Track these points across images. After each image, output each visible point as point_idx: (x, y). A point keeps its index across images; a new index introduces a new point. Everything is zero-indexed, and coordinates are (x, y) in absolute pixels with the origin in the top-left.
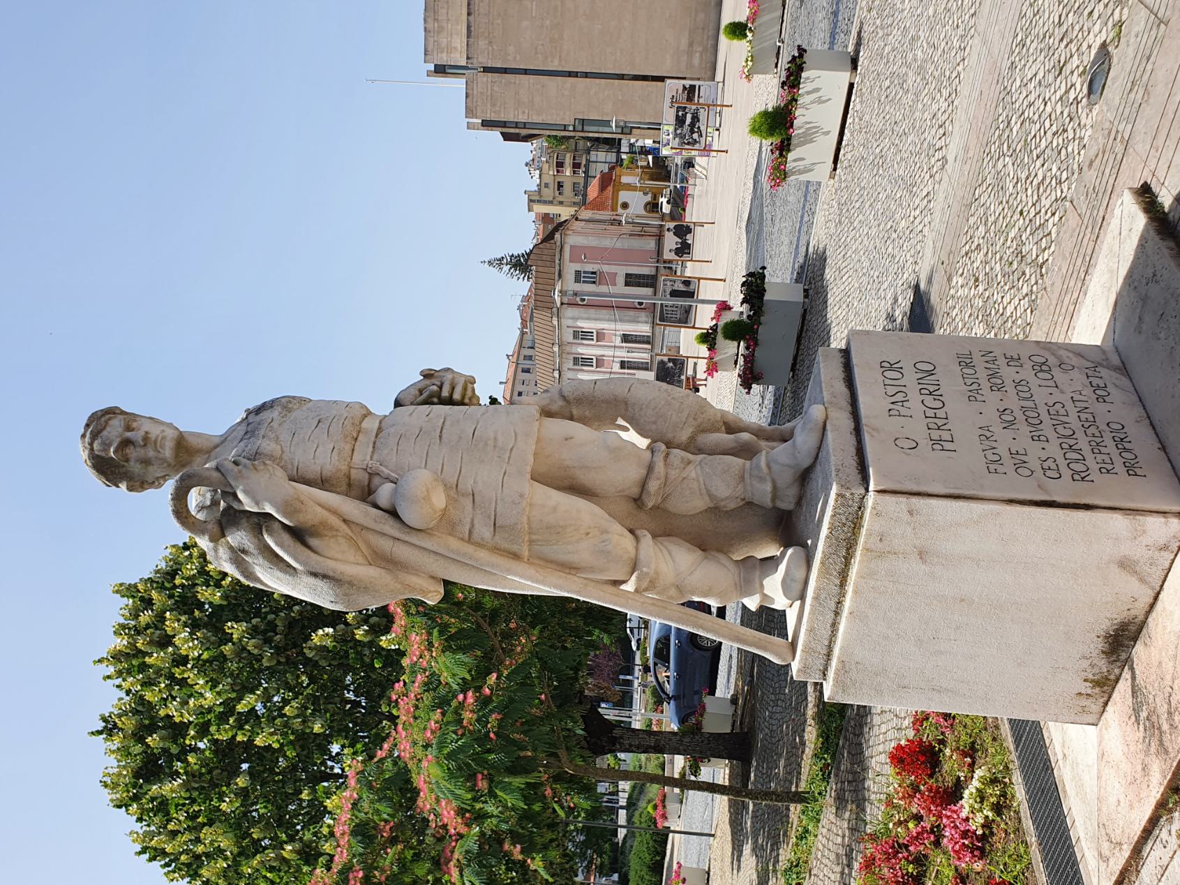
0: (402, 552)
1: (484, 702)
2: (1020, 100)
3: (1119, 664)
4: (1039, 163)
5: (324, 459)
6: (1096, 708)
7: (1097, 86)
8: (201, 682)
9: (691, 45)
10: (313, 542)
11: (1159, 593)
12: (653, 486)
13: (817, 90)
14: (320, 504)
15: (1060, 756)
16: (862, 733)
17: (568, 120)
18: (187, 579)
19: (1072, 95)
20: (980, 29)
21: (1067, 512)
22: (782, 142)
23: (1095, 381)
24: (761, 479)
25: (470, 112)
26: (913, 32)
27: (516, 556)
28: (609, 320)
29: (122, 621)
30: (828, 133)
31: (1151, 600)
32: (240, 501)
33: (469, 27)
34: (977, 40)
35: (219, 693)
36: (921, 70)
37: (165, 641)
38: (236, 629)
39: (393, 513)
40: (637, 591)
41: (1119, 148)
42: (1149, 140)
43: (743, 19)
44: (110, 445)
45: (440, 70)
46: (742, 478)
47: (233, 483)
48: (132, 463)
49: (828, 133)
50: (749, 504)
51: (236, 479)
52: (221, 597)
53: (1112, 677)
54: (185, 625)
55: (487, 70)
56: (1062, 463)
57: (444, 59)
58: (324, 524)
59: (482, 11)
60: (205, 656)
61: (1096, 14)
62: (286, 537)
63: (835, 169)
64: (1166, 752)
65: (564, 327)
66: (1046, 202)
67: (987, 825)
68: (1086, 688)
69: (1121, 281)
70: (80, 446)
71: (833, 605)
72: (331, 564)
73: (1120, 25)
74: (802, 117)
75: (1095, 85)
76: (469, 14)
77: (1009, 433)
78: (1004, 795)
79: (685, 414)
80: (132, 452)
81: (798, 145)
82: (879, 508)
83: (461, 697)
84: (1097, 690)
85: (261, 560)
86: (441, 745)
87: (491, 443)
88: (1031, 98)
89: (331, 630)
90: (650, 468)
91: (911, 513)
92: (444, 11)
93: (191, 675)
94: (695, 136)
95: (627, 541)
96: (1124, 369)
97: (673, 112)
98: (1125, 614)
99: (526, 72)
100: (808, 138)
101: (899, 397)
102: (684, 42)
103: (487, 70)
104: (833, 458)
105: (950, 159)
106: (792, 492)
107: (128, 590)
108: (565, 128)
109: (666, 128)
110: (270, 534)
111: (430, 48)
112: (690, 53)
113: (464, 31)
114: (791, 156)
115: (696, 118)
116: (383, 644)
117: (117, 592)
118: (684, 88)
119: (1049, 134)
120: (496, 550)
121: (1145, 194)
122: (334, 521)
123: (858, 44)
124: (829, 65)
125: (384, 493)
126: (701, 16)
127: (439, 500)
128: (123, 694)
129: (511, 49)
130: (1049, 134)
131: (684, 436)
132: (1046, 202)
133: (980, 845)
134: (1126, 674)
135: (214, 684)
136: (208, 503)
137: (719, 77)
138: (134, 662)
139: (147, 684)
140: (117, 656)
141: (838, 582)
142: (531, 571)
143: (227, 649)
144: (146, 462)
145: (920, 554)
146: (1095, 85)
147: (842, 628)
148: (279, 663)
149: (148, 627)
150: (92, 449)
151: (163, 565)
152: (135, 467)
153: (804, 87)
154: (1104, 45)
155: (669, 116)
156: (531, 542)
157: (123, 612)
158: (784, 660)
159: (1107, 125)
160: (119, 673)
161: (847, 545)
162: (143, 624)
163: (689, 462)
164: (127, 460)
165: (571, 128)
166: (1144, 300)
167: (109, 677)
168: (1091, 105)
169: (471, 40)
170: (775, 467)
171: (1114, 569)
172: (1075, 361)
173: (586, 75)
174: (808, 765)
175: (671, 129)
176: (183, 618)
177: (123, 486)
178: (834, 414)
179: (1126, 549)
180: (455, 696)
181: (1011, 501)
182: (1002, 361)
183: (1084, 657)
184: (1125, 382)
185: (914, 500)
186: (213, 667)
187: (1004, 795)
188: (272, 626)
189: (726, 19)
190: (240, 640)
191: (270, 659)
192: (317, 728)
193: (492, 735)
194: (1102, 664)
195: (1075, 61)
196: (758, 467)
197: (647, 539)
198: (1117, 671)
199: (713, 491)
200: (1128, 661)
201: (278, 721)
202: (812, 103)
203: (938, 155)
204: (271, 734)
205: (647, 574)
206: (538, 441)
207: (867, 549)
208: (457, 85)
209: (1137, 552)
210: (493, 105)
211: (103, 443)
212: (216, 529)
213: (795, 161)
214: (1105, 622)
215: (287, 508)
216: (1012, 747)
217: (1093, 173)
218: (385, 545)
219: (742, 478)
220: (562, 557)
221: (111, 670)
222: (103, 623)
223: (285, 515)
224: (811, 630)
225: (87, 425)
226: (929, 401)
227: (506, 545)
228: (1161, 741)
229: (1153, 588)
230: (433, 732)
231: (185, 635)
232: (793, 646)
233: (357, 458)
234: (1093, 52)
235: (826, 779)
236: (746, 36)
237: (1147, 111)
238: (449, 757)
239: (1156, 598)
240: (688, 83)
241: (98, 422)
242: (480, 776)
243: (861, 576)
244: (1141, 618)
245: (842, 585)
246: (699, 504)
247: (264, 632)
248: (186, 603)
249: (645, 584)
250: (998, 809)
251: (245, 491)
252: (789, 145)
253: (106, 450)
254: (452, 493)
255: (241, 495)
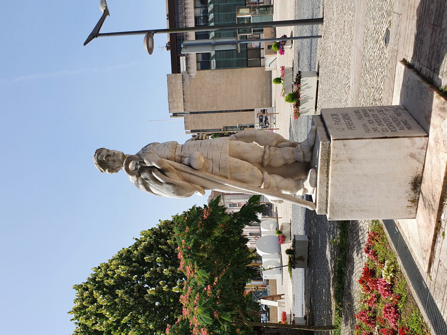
0: (193, 178)
1: (213, 288)
2: (367, 56)
3: (418, 193)
4: (375, 71)
5: (168, 153)
6: (414, 211)
7: (387, 41)
8: (108, 313)
9: (262, 97)
10: (167, 173)
11: (424, 165)
12: (266, 157)
13: (307, 84)
14: (167, 163)
15: (407, 236)
16: (350, 288)
17: (221, 127)
18: (101, 278)
19: (381, 47)
20: (354, 43)
21: (391, 139)
22: (297, 103)
23: (397, 112)
24: (299, 151)
25: (186, 128)
26: (334, 55)
27: (226, 178)
28: (242, 199)
29: (77, 298)
30: (312, 98)
31: (422, 168)
32: (145, 163)
33: (184, 99)
34: (353, 47)
35: (114, 317)
36: (339, 65)
37: (95, 301)
38: (119, 292)
39: (190, 166)
40: (264, 188)
41: (395, 53)
42: (402, 47)
43: (279, 77)
44: (103, 157)
45: (175, 115)
46: (293, 152)
47: (143, 158)
48: (110, 162)
49: (312, 98)
50: (296, 162)
51: (143, 156)
52: (114, 282)
53: (417, 198)
54: (101, 294)
55: (191, 113)
56: (387, 128)
57: (176, 111)
58: (170, 168)
59: (188, 93)
60: (109, 304)
61: (384, 22)
62: (159, 173)
63: (316, 110)
64: (434, 210)
65: (226, 202)
66: (379, 80)
67: (392, 279)
68: (409, 204)
69: (401, 87)
70: (94, 159)
71: (325, 184)
72: (173, 180)
73: (390, 22)
74: (303, 94)
75: (386, 40)
76: (184, 95)
77: (372, 125)
78: (395, 267)
79: (274, 137)
80: (110, 158)
81: (302, 104)
82: (335, 145)
83: (205, 289)
84: (413, 204)
85: (152, 181)
86: (200, 303)
87: (216, 146)
88: (371, 54)
89: (154, 288)
90: (265, 152)
91: (344, 145)
92: (175, 95)
93: (104, 312)
94: (267, 125)
95: (259, 172)
96: (405, 109)
97: (258, 119)
98: (416, 174)
99: (205, 112)
100: (306, 101)
101: (338, 120)
102: (260, 97)
103: (191, 113)
104: (319, 136)
105: (351, 85)
106: (309, 155)
107: (77, 287)
108: (220, 130)
109: (256, 125)
110: (154, 172)
111: (171, 108)
112: (262, 101)
113: (182, 101)
114: (300, 108)
115: (266, 119)
116: (173, 290)
117: (74, 288)
118: (261, 111)
119: (377, 61)
120: (220, 176)
121: (404, 61)
122: (172, 167)
123: (319, 68)
124: (310, 75)
125: (186, 160)
126: (265, 88)
127: (203, 160)
128: (77, 326)
129: (199, 105)
130: (377, 61)
131: (274, 144)
132: (379, 80)
133: (390, 288)
134: (421, 196)
135: (112, 314)
136: (134, 169)
137: (273, 106)
138: (82, 311)
139: (87, 319)
140: (76, 310)
141: (326, 175)
142: (231, 182)
143: (117, 300)
144: (114, 161)
145: (349, 160)
146: (386, 40)
147: (329, 192)
148: (136, 304)
149: (87, 297)
150: (98, 159)
151: (91, 277)
152: (111, 163)
153: (302, 84)
154: (387, 29)
155: (257, 120)
156: (231, 173)
157: (77, 294)
158: (313, 208)
159: (392, 49)
160: (77, 318)
161: (327, 161)
162: (85, 297)
163: (276, 150)
164: (108, 161)
165: (222, 130)
166: (407, 87)
167: (72, 320)
168: (386, 47)
169: (185, 103)
170: (303, 147)
171: (409, 157)
172: (390, 109)
173: (226, 111)
174: (334, 316)
175: (258, 125)
176: (100, 292)
177: (107, 171)
178: (318, 128)
179: (411, 150)
180: (203, 289)
181: (374, 138)
182: (368, 111)
183: (406, 192)
184: (406, 112)
185: (345, 141)
186: (112, 308)
187: (395, 267)
188: (133, 290)
189: (274, 77)
190: (121, 296)
191: (133, 302)
192: (151, 327)
193: (218, 297)
194: (412, 193)
195: (381, 37)
196: (298, 148)
197: (266, 173)
198: (418, 196)
199: (285, 157)
200: (420, 192)
201: (137, 326)
202: (306, 88)
203: (347, 86)
204: (135, 331)
205: (267, 182)
206: (230, 145)
207: (333, 161)
208: (181, 120)
209: (415, 151)
210: (194, 125)
211: (101, 156)
212: (138, 174)
213: (302, 109)
214: (410, 179)
215: (159, 163)
216: (395, 250)
217: (390, 64)
218: (187, 176)
219: (293, 152)
220: (240, 178)
221: (73, 316)
222: (71, 300)
223: (159, 165)
224: (320, 195)
225: (96, 152)
226: (347, 121)
227: (223, 174)
228: (432, 209)
229: (422, 163)
230: (197, 301)
231: (101, 297)
232: (316, 204)
233: (177, 153)
234: (385, 32)
235: (340, 316)
236: (281, 82)
237: (401, 39)
238: (204, 306)
239: (424, 167)
240: (262, 109)
241: (99, 152)
242: (215, 312)
243: (333, 171)
244: (421, 175)
245: (328, 176)
246: (280, 162)
247: (130, 293)
248: (100, 286)
249: (266, 186)
250: (394, 271)
251: (147, 160)
252: (299, 103)
253: (102, 158)
254: (206, 159)
255: (145, 161)
